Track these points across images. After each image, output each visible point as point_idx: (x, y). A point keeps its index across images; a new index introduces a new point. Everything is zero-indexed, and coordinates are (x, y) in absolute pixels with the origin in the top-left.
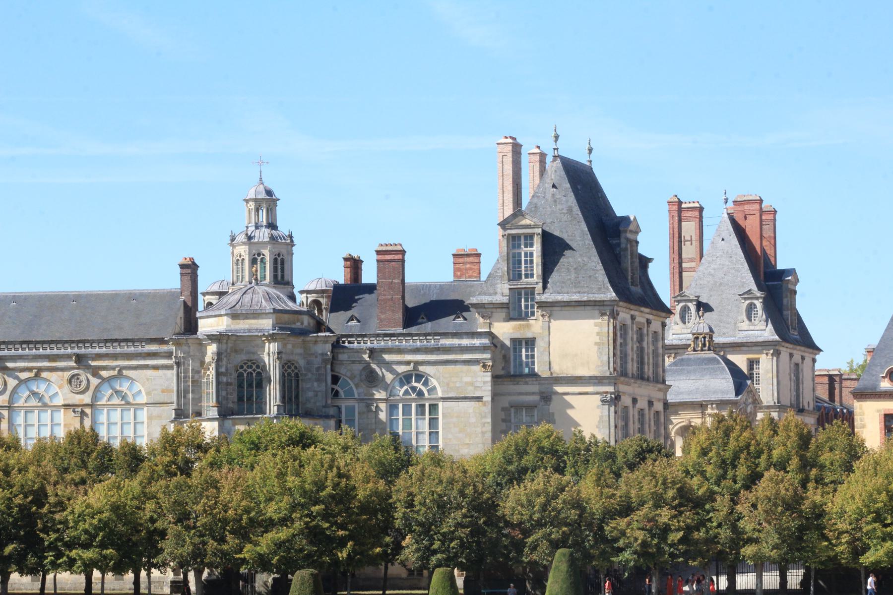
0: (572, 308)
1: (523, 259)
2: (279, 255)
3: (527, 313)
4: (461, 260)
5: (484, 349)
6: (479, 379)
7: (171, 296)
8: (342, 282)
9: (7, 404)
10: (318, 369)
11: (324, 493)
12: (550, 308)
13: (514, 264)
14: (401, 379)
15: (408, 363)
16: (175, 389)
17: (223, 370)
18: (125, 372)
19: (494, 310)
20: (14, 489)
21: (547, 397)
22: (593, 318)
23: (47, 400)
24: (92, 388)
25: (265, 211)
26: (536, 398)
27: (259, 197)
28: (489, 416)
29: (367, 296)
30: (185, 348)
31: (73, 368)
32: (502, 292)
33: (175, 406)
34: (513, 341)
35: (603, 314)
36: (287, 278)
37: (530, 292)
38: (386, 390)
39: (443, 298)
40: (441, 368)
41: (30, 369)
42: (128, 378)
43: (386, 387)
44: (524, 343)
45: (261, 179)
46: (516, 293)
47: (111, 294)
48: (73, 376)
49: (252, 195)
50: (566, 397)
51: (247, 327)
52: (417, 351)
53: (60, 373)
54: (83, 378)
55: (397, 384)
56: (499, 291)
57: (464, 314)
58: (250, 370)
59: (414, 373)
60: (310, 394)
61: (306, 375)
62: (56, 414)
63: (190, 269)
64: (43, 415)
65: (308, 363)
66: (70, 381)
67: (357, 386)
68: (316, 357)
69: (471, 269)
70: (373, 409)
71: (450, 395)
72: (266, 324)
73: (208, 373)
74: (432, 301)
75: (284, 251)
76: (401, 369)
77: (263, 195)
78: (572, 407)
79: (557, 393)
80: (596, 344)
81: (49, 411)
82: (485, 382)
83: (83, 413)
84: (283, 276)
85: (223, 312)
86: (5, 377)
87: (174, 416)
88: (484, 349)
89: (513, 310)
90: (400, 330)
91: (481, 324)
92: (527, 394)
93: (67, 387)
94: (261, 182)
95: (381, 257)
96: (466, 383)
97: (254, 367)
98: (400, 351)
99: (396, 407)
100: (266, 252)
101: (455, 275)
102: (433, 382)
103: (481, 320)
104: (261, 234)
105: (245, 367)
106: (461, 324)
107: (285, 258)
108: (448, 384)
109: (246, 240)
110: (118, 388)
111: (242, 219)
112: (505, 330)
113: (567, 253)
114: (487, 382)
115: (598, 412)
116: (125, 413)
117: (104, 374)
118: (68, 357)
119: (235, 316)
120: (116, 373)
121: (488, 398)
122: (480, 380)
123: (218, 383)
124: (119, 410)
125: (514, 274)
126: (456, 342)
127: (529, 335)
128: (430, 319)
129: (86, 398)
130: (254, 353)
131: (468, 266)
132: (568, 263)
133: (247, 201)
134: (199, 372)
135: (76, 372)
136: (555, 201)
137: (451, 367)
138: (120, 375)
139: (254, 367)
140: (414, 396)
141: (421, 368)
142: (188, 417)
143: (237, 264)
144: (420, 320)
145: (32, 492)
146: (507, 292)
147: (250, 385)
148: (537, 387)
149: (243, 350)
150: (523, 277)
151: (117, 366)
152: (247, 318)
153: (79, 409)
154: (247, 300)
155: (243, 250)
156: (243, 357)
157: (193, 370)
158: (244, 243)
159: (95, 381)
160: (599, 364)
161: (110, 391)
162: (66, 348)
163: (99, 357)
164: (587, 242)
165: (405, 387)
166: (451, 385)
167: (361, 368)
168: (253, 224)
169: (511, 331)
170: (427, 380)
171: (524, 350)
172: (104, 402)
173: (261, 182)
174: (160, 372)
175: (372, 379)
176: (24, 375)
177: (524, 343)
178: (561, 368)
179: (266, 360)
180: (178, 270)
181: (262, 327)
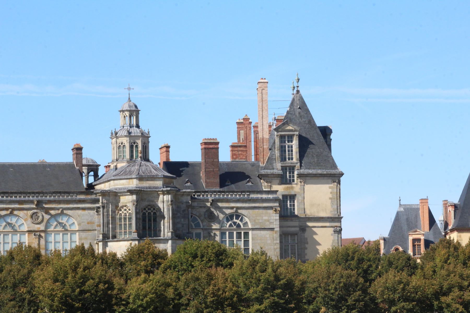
0: (317, 178)
2: (122, 143)
3: (290, 180)
4: (236, 149)
6: (272, 218)
7: (68, 166)
10: (184, 211)
15: (232, 208)
18: (65, 212)
19: (273, 178)
21: (303, 229)
22: (328, 183)
23: (17, 228)
24: (45, 221)
25: (135, 117)
26: (298, 229)
27: (132, 109)
28: (279, 239)
30: (107, 197)
31: (33, 209)
34: (283, 196)
35: (334, 182)
36: (147, 157)
38: (219, 223)
39: (232, 171)
40: (251, 211)
41: (7, 209)
42: (67, 215)
43: (219, 222)
44: (289, 198)
45: (129, 98)
48: (34, 214)
49: (126, 107)
51: (148, 185)
53: (25, 212)
54: (40, 215)
55: (225, 220)
56: (275, 167)
58: (149, 211)
59: (235, 214)
63: (78, 150)
66: (32, 217)
67: (202, 222)
68: (183, 204)
69: (242, 154)
70: (212, 234)
71: (256, 227)
73: (120, 212)
74: (226, 172)
75: (146, 141)
76: (228, 211)
77: (134, 109)
78: (316, 234)
79: (309, 227)
80: (330, 198)
81: (18, 235)
82: (276, 220)
83: (40, 236)
89: (284, 179)
90: (218, 189)
91: (265, 186)
93: (30, 220)
94: (130, 100)
95: (207, 146)
96: (265, 220)
97: (152, 209)
98: (227, 201)
99: (225, 233)
101: (232, 158)
103: (266, 184)
105: (147, 209)
108: (255, 221)
109: (128, 134)
110: (60, 221)
111: (120, 122)
112: (281, 189)
113: (311, 146)
115: (332, 238)
116: (65, 236)
117: (52, 212)
118: (32, 202)
119: (141, 178)
121: (277, 229)
122: (273, 218)
124: (61, 234)
125: (283, 159)
127: (293, 193)
128: (233, 183)
129: (42, 227)
131: (240, 152)
133: (123, 111)
134: (115, 212)
135: (35, 211)
136: (301, 117)
137: (256, 211)
138: (62, 213)
139: (152, 209)
140: (235, 227)
141: (240, 211)
143: (119, 149)
144: (227, 184)
146: (280, 168)
147: (150, 220)
150: (287, 159)
151: (61, 208)
152: (148, 180)
154: (143, 169)
155: (126, 141)
156: (146, 203)
157: (111, 210)
158: (126, 136)
159: (47, 217)
160: (332, 210)
161: (55, 223)
162: (24, 197)
163: (50, 202)
164: (321, 140)
165: (230, 222)
166: (257, 221)
167: (205, 211)
168: (128, 125)
169: (283, 190)
170: (242, 218)
171: (288, 202)
173: (130, 100)
174: (86, 212)
175: (212, 218)
177: (289, 198)
178: (310, 212)
180: (230, 149)
181: (156, 185)
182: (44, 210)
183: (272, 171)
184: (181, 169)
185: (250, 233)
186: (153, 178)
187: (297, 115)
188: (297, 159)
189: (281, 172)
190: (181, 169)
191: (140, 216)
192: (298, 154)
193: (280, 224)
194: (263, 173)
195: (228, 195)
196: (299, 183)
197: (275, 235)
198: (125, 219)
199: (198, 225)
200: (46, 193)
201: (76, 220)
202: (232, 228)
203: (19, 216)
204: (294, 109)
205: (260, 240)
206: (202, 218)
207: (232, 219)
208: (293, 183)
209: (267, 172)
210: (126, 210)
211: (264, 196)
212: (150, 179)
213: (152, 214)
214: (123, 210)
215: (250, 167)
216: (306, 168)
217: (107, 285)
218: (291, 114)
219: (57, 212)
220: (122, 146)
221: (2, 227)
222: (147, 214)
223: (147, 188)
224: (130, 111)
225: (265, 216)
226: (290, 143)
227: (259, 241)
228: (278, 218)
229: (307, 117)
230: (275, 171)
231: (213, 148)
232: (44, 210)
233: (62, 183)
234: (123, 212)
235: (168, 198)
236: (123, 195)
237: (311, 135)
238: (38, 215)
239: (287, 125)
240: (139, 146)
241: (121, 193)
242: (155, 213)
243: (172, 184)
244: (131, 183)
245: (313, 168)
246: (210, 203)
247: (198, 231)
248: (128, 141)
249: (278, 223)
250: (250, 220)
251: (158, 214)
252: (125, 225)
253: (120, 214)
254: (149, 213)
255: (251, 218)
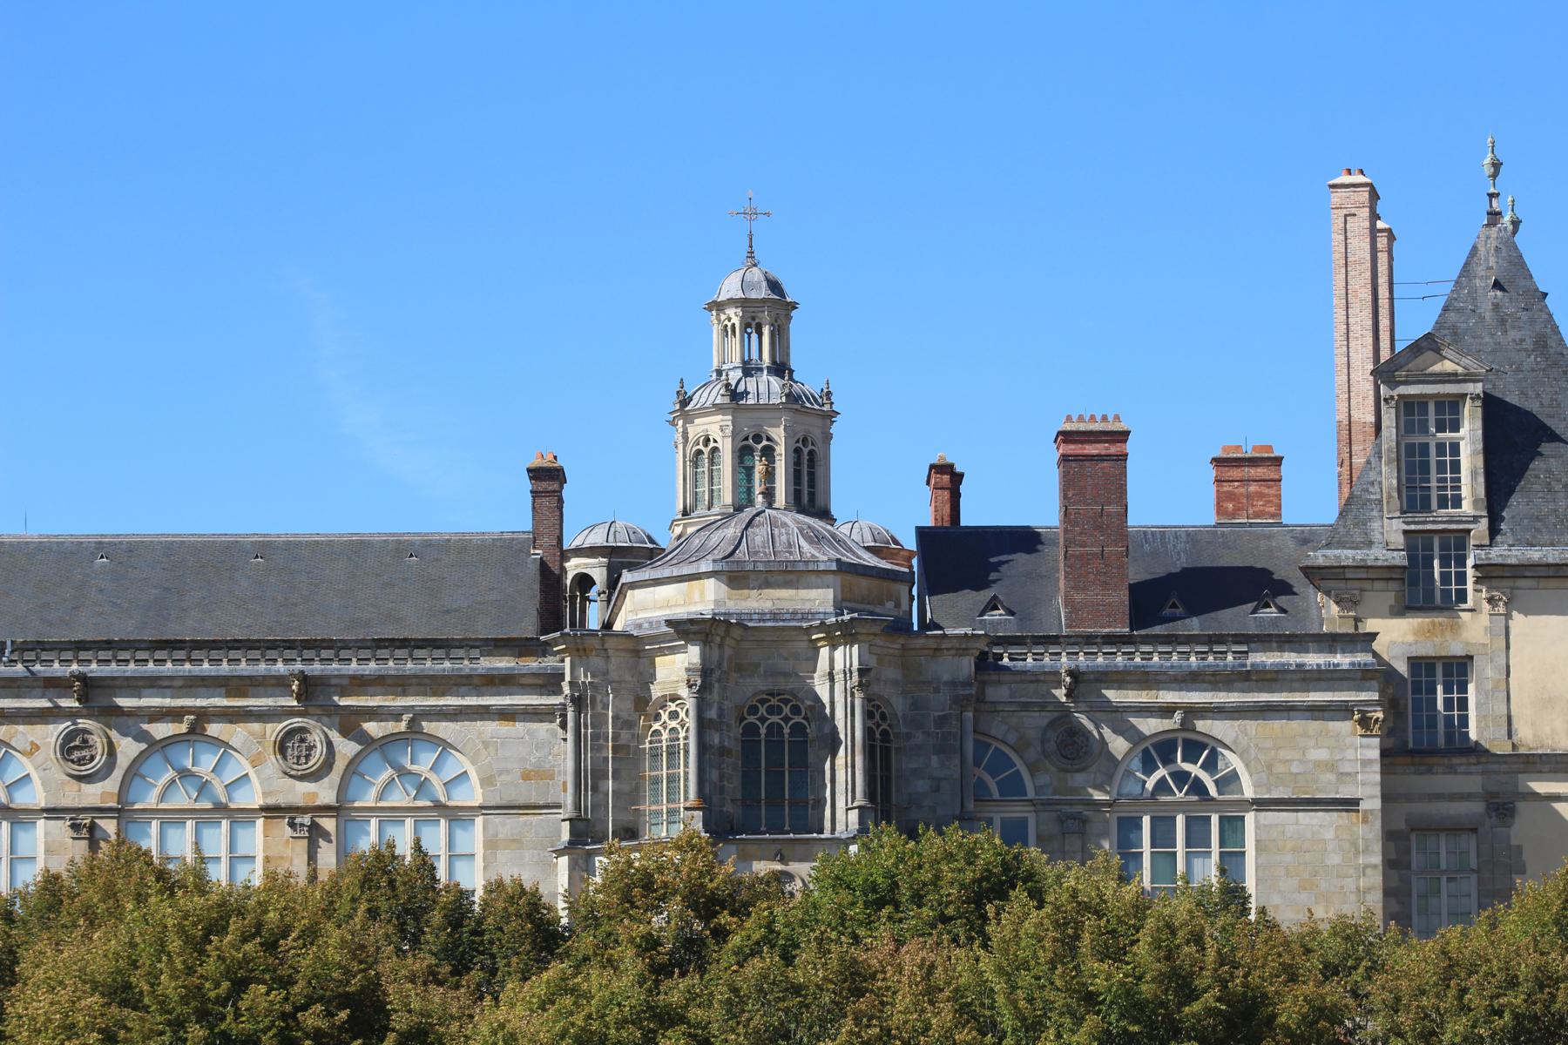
1: (1433, 458)
2: (805, 441)
3: (1446, 594)
4: (1236, 473)
5: (1358, 677)
6: (1350, 754)
7: (504, 549)
8: (928, 521)
9: (113, 804)
10: (942, 721)
11: (1196, 1007)
12: (1510, 583)
13: (1410, 469)
14: (1146, 752)
15: (1167, 711)
16: (570, 765)
17: (712, 714)
18: (427, 726)
19: (1367, 585)
20: (296, 989)
21: (1503, 807)
24: (340, 765)
26: (1477, 807)
27: (754, 295)
29: (1020, 558)
30: (597, 661)
32: (1388, 537)
33: (568, 810)
34: (1415, 662)
36: (820, 501)
37: (1455, 543)
39: (1206, 563)
40: (1251, 726)
41: (175, 715)
46: (1417, 543)
47: (351, 543)
48: (290, 734)
49: (731, 288)
50: (1558, 806)
51: (767, 606)
52: (1192, 679)
53: (256, 727)
54: (316, 738)
55: (1136, 764)
56: (1376, 537)
57: (1282, 600)
58: (775, 719)
60: (921, 786)
61: (909, 736)
62: (242, 833)
64: (208, 833)
65: (915, 705)
66: (282, 748)
67: (1033, 769)
68: (937, 690)
69: (1260, 495)
71: (1275, 795)
72: (819, 600)
73: (656, 726)
74: (1184, 569)
75: (816, 433)
76: (1150, 726)
77: (763, 292)
82: (1365, 763)
83: (316, 832)
84: (812, 495)
85: (705, 566)
86: (114, 734)
87: (565, 836)
88: (1358, 677)
89: (1419, 584)
91: (1331, 614)
92: (1452, 797)
93: (273, 762)
97: (786, 710)
98: (1146, 679)
100: (778, 434)
101: (1220, 510)
102: (1232, 761)
104: (763, 388)
105: (763, 711)
106: (1274, 621)
107: (819, 450)
108: (1270, 767)
109: (727, 400)
112: (1398, 637)
114: (1370, 761)
117: (373, 728)
118: (279, 684)
119: (736, 576)
120: (402, 726)
121: (1372, 803)
122: (1351, 756)
123: (702, 747)
125: (1414, 498)
126: (1291, 658)
127: (1457, 649)
128: (1194, 610)
129: (324, 792)
130: (786, 675)
131: (1253, 488)
132: (1549, 471)
133: (718, 306)
134: (630, 725)
135: (297, 722)
136: (1503, 322)
137: (1277, 725)
138: (414, 735)
139: (786, 710)
141: (1202, 725)
142: (601, 838)
143: (696, 464)
144: (1167, 611)
145: (345, 1000)
146: (1399, 540)
148: (1479, 779)
149: (758, 665)
150: (1434, 504)
153: (306, 820)
154: (758, 540)
155: (717, 428)
158: (719, 409)
159: (346, 748)
161: (170, 774)
163: (360, 684)
166: (1279, 768)
167: (1046, 721)
168: (737, 362)
170: (1214, 756)
171: (1440, 688)
172: (369, 799)
174: (519, 727)
175: (1074, 748)
176: (161, 730)
178: (1539, 730)
179: (823, 692)
180: (527, 485)
181: (807, 607)
182: (337, 719)
183: (1359, 555)
184: (992, 560)
185: (1250, 818)
186: (792, 575)
187: (1488, 315)
188: (1476, 502)
189: (1400, 558)
190: (992, 560)
191: (731, 737)
192: (1481, 479)
193: (1383, 784)
194: (1321, 561)
195: (1147, 656)
196: (1486, 606)
197: (1361, 830)
198: (672, 752)
199: (1012, 787)
200: (345, 645)
201: (473, 763)
202: (1169, 798)
203: (226, 745)
204: (1473, 292)
205: (1294, 850)
206: (1032, 754)
207: (1168, 760)
208: (1463, 606)
209: (1337, 558)
210: (674, 715)
211: (1313, 659)
212: (780, 578)
213: (787, 731)
214: (665, 717)
215: (1291, 544)
216: (1518, 542)
217: (343, 1015)
218: (1458, 310)
219: (391, 727)
220: (706, 451)
221: (156, 792)
222: (763, 731)
223: (762, 616)
224: (743, 303)
225: (1317, 746)
226: (1448, 434)
227: (1288, 858)
228: (1375, 754)
229: (1532, 321)
230: (1377, 555)
231: (1100, 458)
232: (337, 719)
233: (448, 612)
234: (663, 725)
235: (846, 657)
236: (662, 652)
237: (1546, 402)
238: (310, 738)
239: (1430, 355)
240: (794, 453)
241: (653, 639)
242: (798, 729)
243: (890, 605)
244: (696, 598)
245: (1546, 538)
246: (1064, 691)
247: (1017, 811)
248: (729, 431)
249: (1378, 778)
250: (1247, 766)
251: (811, 731)
252: (672, 779)
253: (657, 732)
254: (770, 728)
255: (1253, 753)
